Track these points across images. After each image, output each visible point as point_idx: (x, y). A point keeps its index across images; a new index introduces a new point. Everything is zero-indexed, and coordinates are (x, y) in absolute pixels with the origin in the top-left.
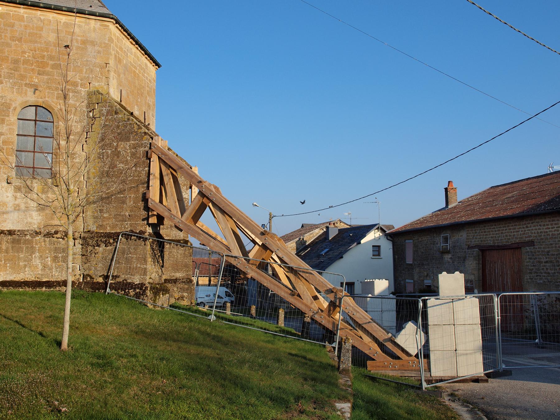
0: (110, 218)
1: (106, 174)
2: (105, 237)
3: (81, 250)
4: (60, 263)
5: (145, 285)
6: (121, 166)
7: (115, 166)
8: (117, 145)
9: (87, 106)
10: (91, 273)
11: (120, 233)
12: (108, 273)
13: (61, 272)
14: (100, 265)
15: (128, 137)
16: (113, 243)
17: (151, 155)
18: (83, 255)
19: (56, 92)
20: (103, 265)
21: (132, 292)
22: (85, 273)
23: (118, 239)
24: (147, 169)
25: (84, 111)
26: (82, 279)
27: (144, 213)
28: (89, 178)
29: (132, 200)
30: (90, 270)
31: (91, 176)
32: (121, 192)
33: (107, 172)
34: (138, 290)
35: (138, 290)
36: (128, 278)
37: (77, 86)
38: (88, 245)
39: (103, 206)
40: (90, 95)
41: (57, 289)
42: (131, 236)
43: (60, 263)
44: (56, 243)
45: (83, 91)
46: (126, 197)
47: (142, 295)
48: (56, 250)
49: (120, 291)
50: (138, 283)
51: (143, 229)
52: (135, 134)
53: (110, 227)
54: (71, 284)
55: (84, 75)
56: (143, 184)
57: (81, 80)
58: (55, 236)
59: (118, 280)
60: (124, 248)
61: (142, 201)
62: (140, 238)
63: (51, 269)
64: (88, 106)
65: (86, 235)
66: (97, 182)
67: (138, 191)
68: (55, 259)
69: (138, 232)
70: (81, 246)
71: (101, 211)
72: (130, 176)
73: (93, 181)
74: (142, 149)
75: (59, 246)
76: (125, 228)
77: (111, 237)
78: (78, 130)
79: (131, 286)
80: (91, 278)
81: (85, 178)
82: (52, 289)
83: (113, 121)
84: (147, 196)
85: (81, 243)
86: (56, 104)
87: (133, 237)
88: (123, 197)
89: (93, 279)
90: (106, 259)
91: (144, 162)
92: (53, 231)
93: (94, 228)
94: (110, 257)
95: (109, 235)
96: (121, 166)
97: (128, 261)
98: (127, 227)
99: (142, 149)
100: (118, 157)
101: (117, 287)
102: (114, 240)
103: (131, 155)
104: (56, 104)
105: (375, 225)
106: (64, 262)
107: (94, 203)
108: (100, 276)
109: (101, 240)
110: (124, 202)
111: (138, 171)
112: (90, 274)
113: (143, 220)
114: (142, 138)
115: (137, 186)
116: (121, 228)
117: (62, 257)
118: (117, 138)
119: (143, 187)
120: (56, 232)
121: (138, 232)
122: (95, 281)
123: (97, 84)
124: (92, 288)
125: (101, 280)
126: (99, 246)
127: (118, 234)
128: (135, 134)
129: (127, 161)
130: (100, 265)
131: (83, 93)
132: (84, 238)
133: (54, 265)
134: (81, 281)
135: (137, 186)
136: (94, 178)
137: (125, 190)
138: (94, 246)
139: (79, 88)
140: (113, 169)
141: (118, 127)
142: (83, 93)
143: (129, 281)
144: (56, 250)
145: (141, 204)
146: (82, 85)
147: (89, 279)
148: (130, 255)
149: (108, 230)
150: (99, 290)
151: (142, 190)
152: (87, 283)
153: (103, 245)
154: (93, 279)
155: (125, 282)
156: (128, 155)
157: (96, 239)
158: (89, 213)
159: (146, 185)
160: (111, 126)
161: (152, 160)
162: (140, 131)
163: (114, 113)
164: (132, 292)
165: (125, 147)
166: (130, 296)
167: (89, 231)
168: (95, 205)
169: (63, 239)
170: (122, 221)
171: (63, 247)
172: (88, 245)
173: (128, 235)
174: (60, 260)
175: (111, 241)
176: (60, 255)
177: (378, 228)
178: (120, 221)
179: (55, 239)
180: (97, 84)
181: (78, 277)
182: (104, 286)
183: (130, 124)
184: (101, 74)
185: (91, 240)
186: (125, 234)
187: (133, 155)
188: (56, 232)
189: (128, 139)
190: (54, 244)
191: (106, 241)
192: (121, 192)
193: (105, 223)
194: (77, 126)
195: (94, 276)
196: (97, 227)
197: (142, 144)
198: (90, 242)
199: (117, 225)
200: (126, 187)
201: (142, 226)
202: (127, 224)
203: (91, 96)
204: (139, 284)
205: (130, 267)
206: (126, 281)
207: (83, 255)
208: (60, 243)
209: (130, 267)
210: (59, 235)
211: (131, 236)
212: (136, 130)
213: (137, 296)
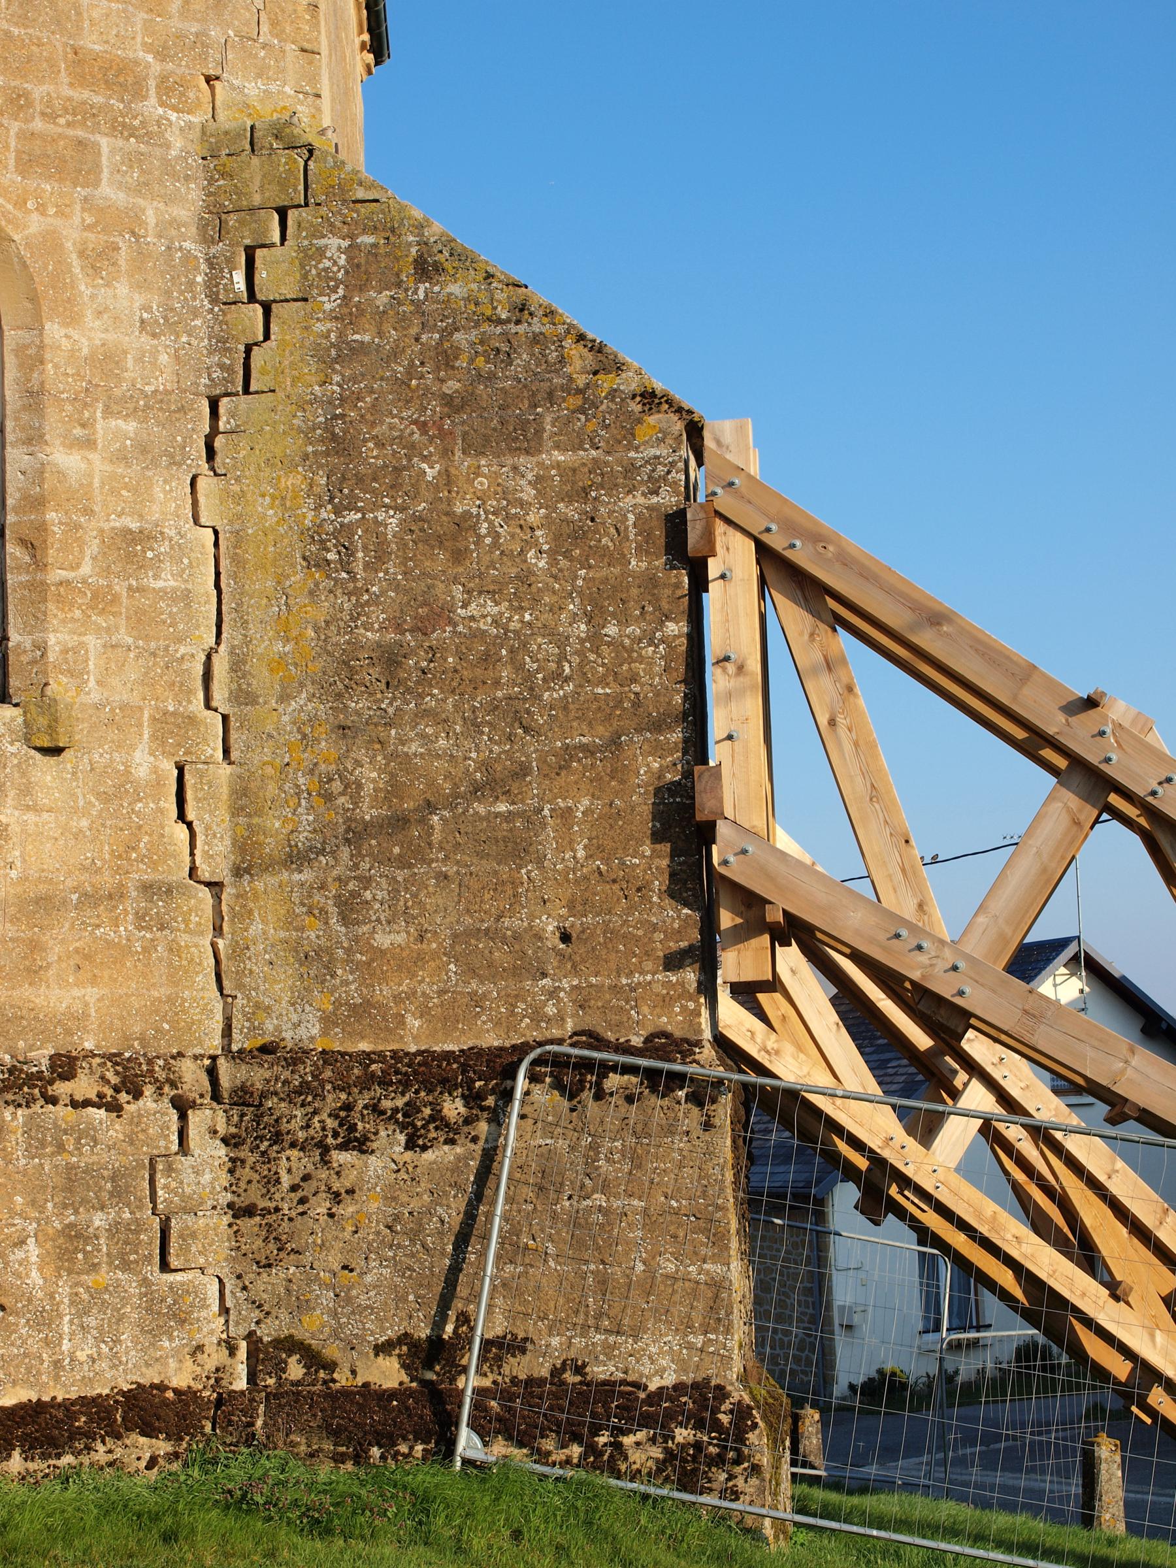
0: (420, 959)
1: (371, 674)
2: (405, 1085)
3: (224, 1179)
4: (104, 1276)
5: (721, 1393)
6: (484, 612)
7: (443, 614)
8: (446, 474)
9: (203, 227)
10: (312, 1327)
11: (522, 1050)
12: (439, 1323)
13: (109, 1335)
14: (377, 1273)
15: (523, 425)
16: (468, 1121)
17: (709, 537)
18: (241, 1212)
19: (15, 127)
20: (402, 1270)
21: (641, 1451)
22: (267, 1333)
23: (507, 1096)
24: (676, 628)
25: (188, 257)
26: (242, 1370)
27: (676, 921)
28: (243, 697)
29: (587, 831)
30: (302, 1306)
31: (262, 679)
32: (492, 784)
33: (391, 659)
34: (683, 1435)
35: (683, 1435)
36: (590, 1349)
37: (139, 93)
38: (277, 1138)
39: (366, 882)
40: (223, 153)
41: (100, 1453)
42: (605, 1069)
43: (104, 1276)
44: (70, 1143)
45: (180, 130)
46: (532, 818)
47: (719, 1461)
48: (74, 1186)
49: (548, 1444)
50: (669, 1380)
51: (672, 1022)
52: (575, 401)
53: (424, 1012)
54: (1011, 1482)
55: (176, 24)
56: (658, 726)
57: (162, 55)
58: (61, 1088)
59: (518, 1367)
60: (549, 1154)
61: (657, 837)
62: (660, 1082)
63: (45, 1320)
64: (215, 223)
65: (258, 1076)
66: (313, 720)
67: (618, 773)
68: (70, 1247)
69: (637, 1041)
70: (222, 1151)
71: (350, 908)
72: (557, 676)
73: (285, 716)
74: (633, 503)
75: (87, 1157)
76: (537, 1016)
77: (448, 1085)
78: (162, 381)
79: (625, 1404)
80: (313, 1359)
81: (219, 695)
82: (68, 1459)
83: (402, 322)
84: (704, 810)
85: (222, 1129)
86: (21, 204)
87: (613, 1081)
88: (509, 817)
89: (331, 1366)
90: (415, 1234)
91: (650, 582)
92: (41, 1057)
93: (304, 1028)
94: (452, 1211)
95: (429, 1072)
96: (484, 612)
97: (589, 1238)
98: (553, 1012)
99: (633, 503)
100: (458, 556)
101: (520, 1414)
102: (473, 1099)
103: (557, 538)
104: (21, 204)
105: (1060, 945)
106: (126, 1266)
107: (296, 858)
108: (382, 1349)
109: (376, 1109)
110: (517, 848)
111: (615, 644)
112: (299, 1334)
113: (673, 962)
114: (628, 435)
115: (614, 743)
116: (509, 1022)
117: (114, 1229)
118: (443, 434)
119: (658, 750)
120: (65, 1066)
121: (637, 1041)
122: (342, 1378)
123: (253, 89)
124: (335, 1434)
125: (388, 1373)
126: (361, 1144)
127: (501, 1066)
128: (575, 401)
129: (525, 577)
130: (377, 1273)
131: (177, 144)
132: (243, 1097)
133: (64, 1290)
134: (241, 1384)
135: (614, 743)
136: (284, 698)
137: (523, 771)
138: (326, 1150)
139: (151, 107)
140: (421, 630)
141: (445, 358)
142: (177, 144)
143: (600, 1371)
144: (74, 1186)
145: (651, 862)
146: (166, 87)
147: (295, 1370)
148: (599, 1199)
149: (415, 1035)
150: (387, 1440)
151: (653, 763)
152: (286, 1401)
153: (390, 1143)
154: (331, 1366)
155: (570, 1378)
156: (532, 543)
157: (333, 1100)
158: (263, 929)
159: (676, 736)
160: (395, 354)
161: (714, 568)
162: (606, 382)
163: (407, 272)
164: (641, 1451)
165: (507, 492)
166: (634, 1476)
167: (265, 1049)
168: (307, 876)
169: (115, 1108)
170: (516, 972)
171: (115, 1160)
172: (277, 1138)
173: (586, 1065)
174: (102, 1257)
175: (454, 1108)
176: (99, 1220)
177: (1075, 958)
178: (493, 972)
179: (62, 1112)
180: (253, 89)
181: (215, 1357)
182: (429, 1414)
183: (536, 339)
184: (274, 23)
185: (288, 1108)
186: (559, 1063)
187: (572, 539)
188: (65, 1066)
189: (522, 438)
190: (61, 1148)
191: (411, 1109)
192: (492, 784)
193: (383, 993)
194: (155, 353)
195: (332, 1351)
196: (328, 1021)
197: (631, 469)
198: (295, 1121)
199: (477, 1000)
200: (531, 750)
201: (665, 1002)
202: (553, 993)
203: (232, 163)
204: (679, 1388)
205: (603, 1282)
206: (579, 1370)
207: (241, 1212)
208: (90, 1135)
209: (603, 1282)
210: (84, 1086)
211: (605, 1069)
212: (581, 381)
213: (685, 1470)
